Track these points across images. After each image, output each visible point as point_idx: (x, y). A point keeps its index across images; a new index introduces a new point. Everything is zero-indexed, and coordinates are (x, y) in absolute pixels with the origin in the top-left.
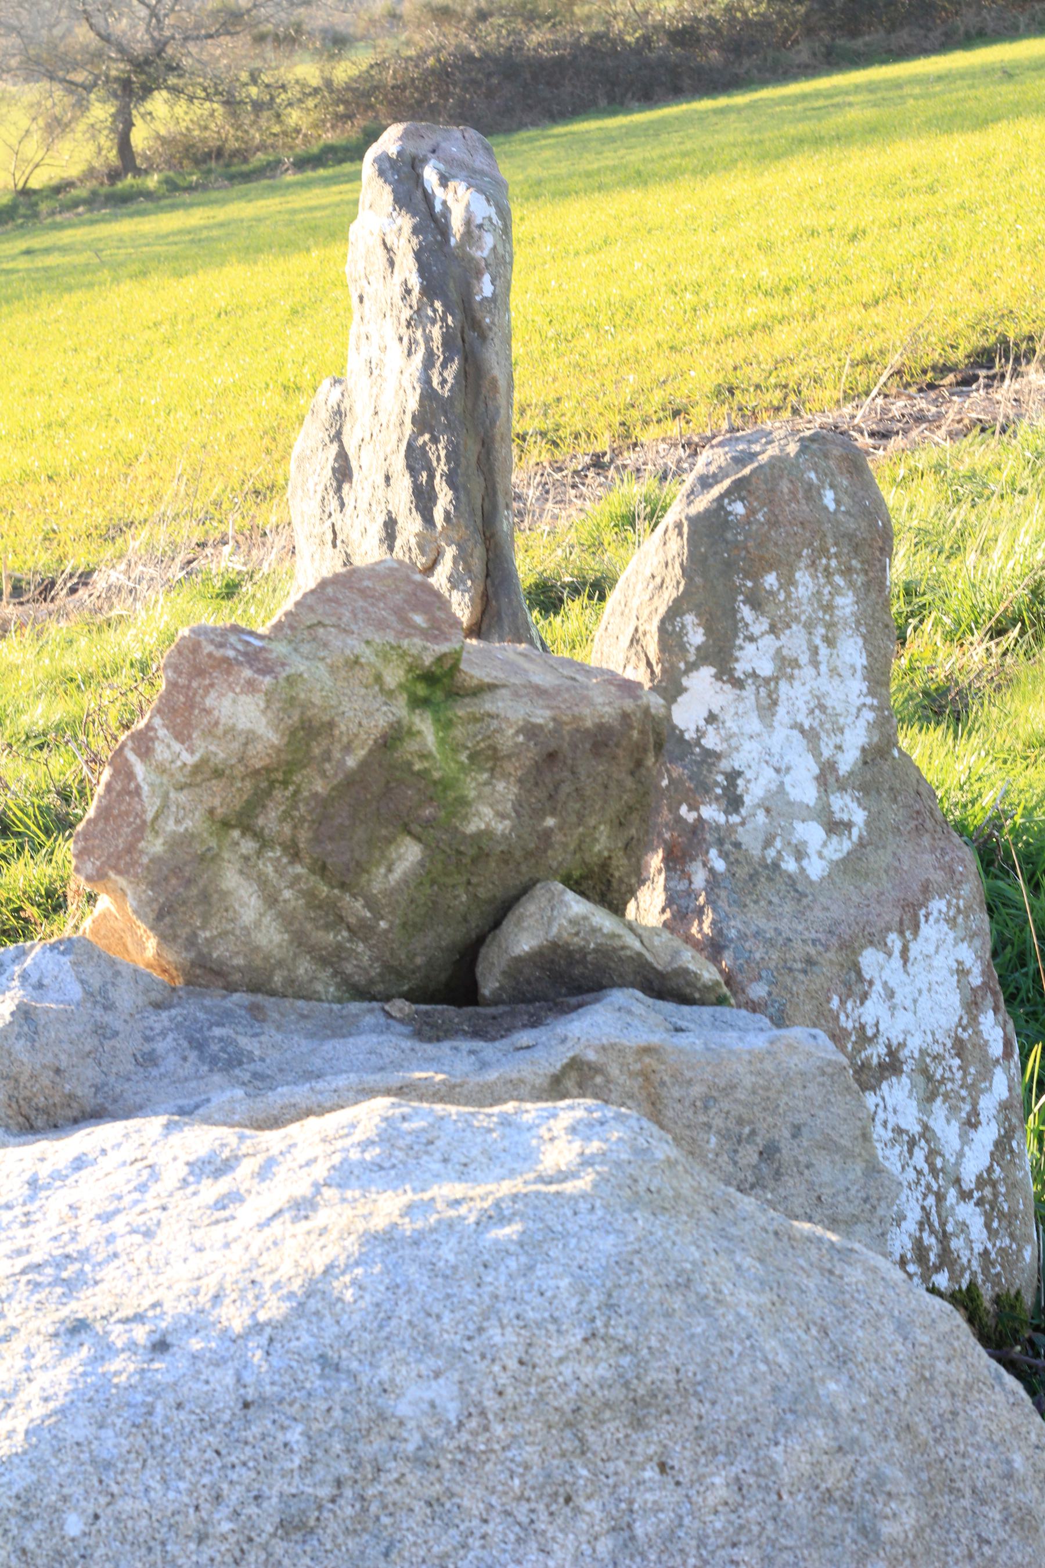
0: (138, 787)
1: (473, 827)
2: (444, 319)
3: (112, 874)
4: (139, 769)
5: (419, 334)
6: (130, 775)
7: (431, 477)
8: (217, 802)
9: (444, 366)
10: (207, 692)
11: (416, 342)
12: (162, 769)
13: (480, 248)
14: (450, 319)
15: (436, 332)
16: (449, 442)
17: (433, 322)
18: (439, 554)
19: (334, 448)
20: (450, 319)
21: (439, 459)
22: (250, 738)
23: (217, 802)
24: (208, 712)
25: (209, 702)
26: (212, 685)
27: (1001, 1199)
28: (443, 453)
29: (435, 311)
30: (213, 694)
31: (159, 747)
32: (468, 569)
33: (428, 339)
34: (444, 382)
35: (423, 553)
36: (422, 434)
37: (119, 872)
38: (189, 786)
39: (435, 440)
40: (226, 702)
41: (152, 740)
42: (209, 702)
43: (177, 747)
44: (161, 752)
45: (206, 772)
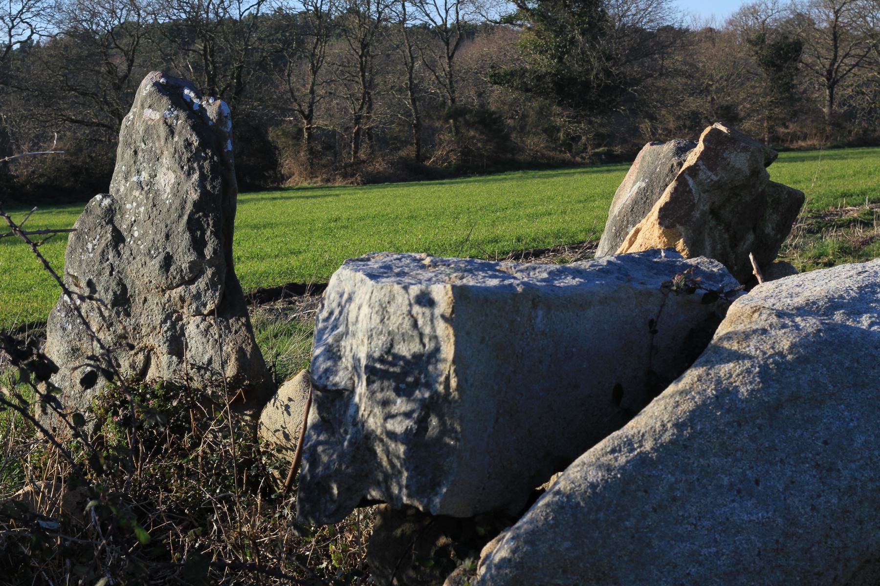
0: (691, 190)
1: (766, 232)
2: (212, 158)
3: (678, 226)
4: (691, 182)
5: (195, 165)
6: (687, 185)
7: (203, 234)
8: (716, 199)
9: (213, 180)
10: (724, 151)
11: (194, 169)
12: (700, 183)
13: (226, 127)
14: (215, 158)
15: (207, 164)
16: (215, 216)
17: (205, 159)
18: (201, 272)
19: (109, 228)
20: (215, 158)
21: (208, 225)
22: (739, 171)
23: (716, 199)
24: (725, 159)
25: (725, 155)
26: (727, 149)
27: (754, 518)
28: (211, 223)
29: (206, 154)
30: (727, 152)
31: (701, 173)
32: (220, 279)
33: (201, 168)
34: (214, 187)
35: (191, 271)
36: (197, 212)
37: (681, 224)
38: (708, 191)
39: (206, 216)
40: (733, 156)
41: (698, 170)
42: (725, 155)
43: (710, 174)
44: (702, 176)
45: (718, 186)
